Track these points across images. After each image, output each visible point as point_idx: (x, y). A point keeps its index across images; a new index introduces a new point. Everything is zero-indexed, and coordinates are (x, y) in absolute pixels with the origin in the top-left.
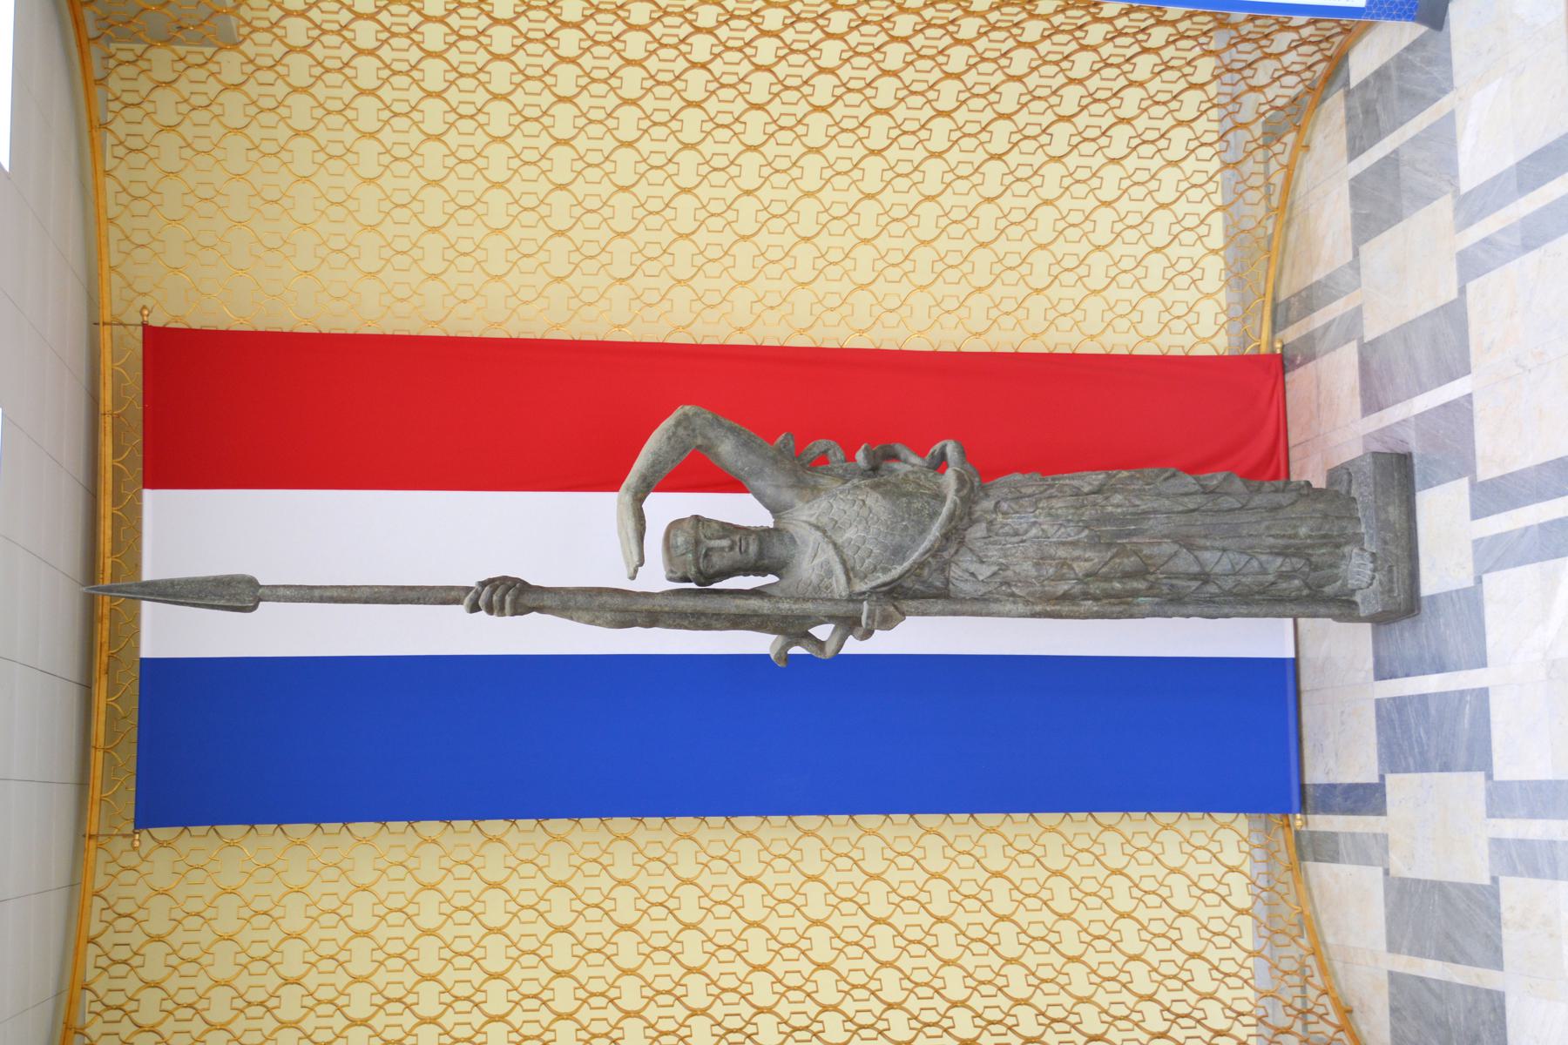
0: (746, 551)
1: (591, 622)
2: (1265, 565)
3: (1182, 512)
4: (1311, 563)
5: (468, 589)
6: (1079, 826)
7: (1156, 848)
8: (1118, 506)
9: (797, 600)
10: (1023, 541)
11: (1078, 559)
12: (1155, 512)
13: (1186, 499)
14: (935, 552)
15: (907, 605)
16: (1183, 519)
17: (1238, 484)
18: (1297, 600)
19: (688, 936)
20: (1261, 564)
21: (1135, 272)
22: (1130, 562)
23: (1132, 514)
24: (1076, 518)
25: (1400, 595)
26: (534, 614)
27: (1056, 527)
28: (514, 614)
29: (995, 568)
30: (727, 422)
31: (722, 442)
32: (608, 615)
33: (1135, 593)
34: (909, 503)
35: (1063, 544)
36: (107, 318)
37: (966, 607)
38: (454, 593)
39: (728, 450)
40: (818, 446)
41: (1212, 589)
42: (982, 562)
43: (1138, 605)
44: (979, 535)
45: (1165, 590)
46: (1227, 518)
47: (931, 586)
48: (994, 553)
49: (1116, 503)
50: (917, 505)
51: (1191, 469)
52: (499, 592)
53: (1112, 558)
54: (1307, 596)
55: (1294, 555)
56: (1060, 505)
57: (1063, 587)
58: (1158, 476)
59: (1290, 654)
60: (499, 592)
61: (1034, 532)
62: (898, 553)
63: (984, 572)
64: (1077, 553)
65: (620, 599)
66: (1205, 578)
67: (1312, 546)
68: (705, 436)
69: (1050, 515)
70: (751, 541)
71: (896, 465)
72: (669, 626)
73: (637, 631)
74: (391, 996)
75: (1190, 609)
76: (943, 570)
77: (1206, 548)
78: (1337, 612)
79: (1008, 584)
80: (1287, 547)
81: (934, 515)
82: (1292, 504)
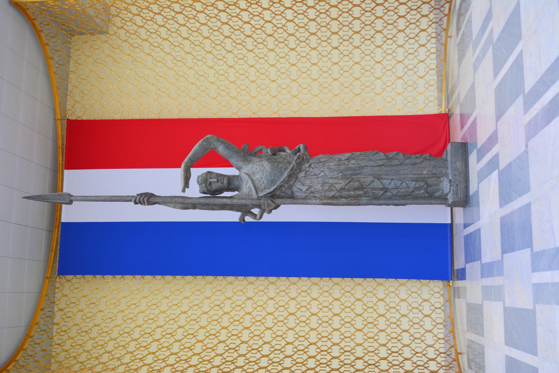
0: (223, 182)
1: (174, 207)
2: (409, 185)
3: (377, 166)
4: (427, 184)
5: (134, 196)
6: (369, 283)
7: (419, 292)
8: (353, 164)
9: (239, 199)
10: (318, 178)
11: (336, 183)
12: (367, 166)
13: (379, 162)
14: (286, 181)
15: (278, 201)
16: (378, 168)
17: (401, 156)
18: (424, 198)
19: (403, 319)
20: (407, 184)
21: (392, 86)
22: (356, 184)
23: (358, 167)
24: (338, 169)
25: (461, 195)
26: (157, 205)
27: (330, 172)
28: (148, 205)
29: (307, 187)
30: (222, 140)
31: (219, 146)
32: (179, 205)
33: (360, 196)
34: (278, 165)
35: (331, 178)
36: (59, 118)
37: (298, 201)
38: (129, 198)
39: (221, 150)
40: (258, 148)
41: (389, 194)
42: (303, 185)
43: (362, 200)
44: (302, 176)
45: (371, 194)
46: (395, 168)
47: (287, 194)
48: (308, 182)
49: (353, 163)
50: (281, 166)
51: (384, 151)
52: (142, 197)
53: (348, 183)
54: (428, 196)
55: (420, 181)
56: (332, 164)
57: (332, 194)
58: (371, 154)
59: (449, 222)
60: (142, 197)
61: (322, 174)
62: (273, 182)
63: (304, 188)
64: (336, 181)
65: (181, 199)
66: (385, 190)
67: (428, 178)
68: (214, 145)
69: (328, 168)
70: (225, 179)
71: (282, 153)
72: (200, 209)
73: (197, 211)
74: (301, 335)
75: (382, 202)
76: (291, 189)
77: (385, 179)
78: (439, 202)
79: (313, 193)
80: (418, 178)
81: (287, 168)
82: (421, 162)
